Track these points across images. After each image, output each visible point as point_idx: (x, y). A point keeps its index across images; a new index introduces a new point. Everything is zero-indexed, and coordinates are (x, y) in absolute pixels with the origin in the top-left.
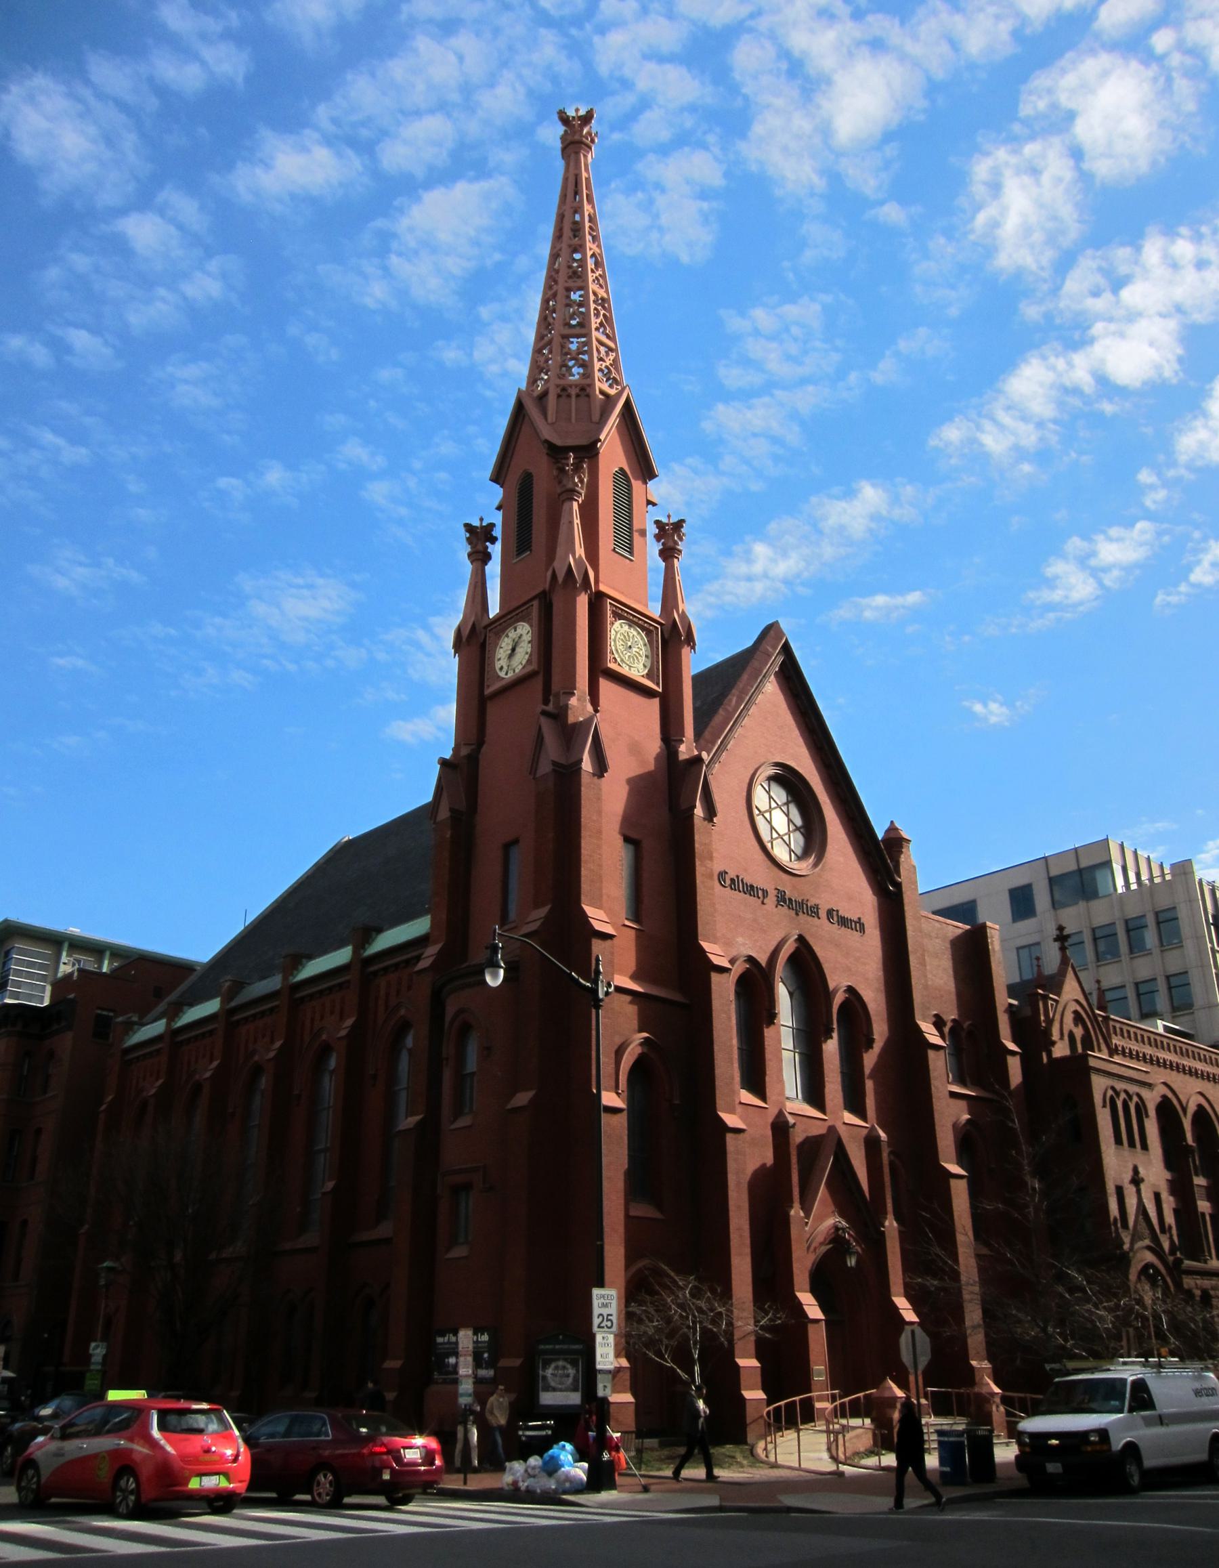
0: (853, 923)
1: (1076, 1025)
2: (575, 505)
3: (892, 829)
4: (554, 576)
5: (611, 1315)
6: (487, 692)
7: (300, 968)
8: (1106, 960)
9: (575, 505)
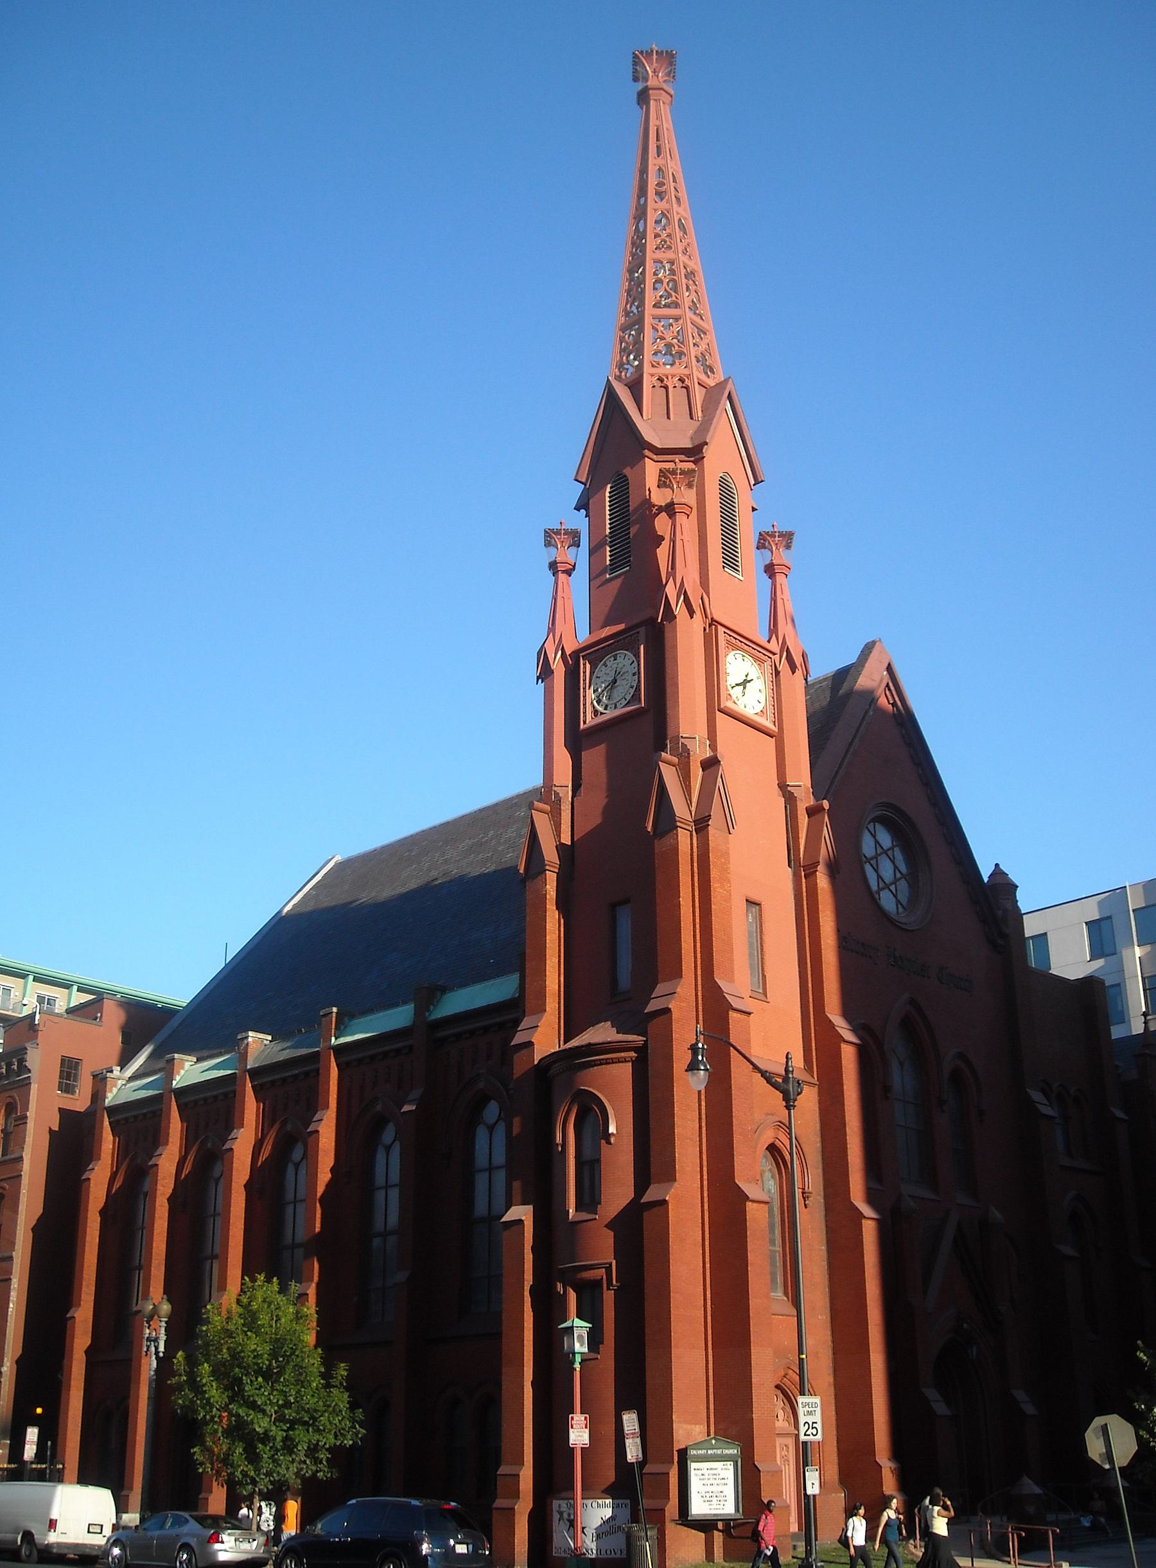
3: (998, 872)
5: (816, 1423)
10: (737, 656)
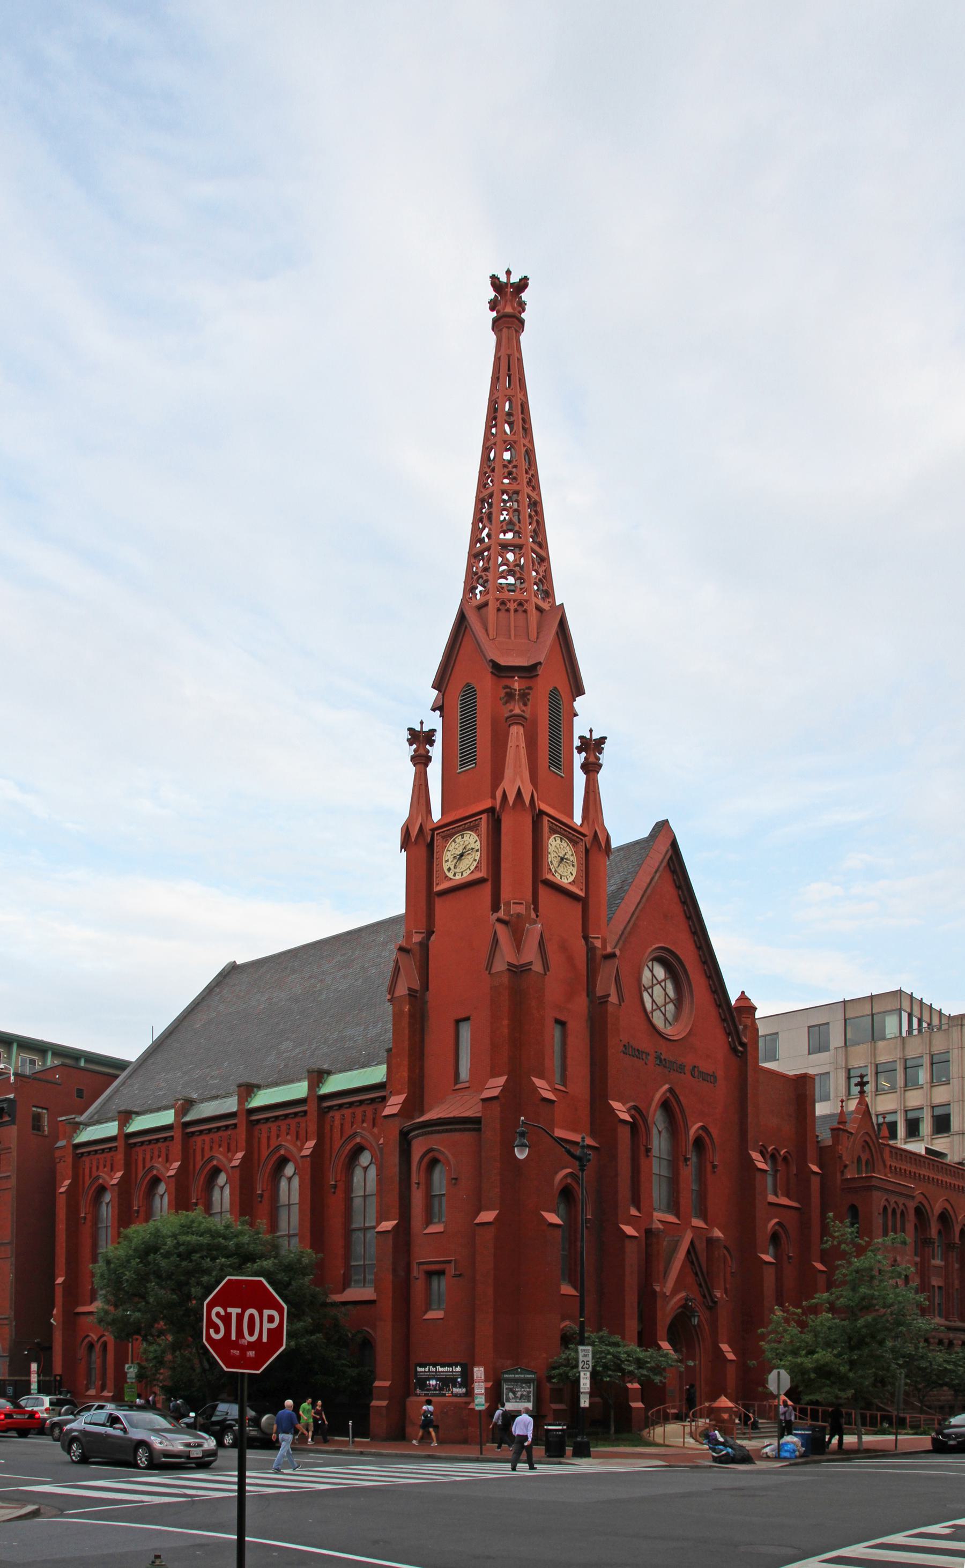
1: (864, 1151)
3: (743, 997)
4: (504, 796)
7: (253, 1095)
10: (557, 838)
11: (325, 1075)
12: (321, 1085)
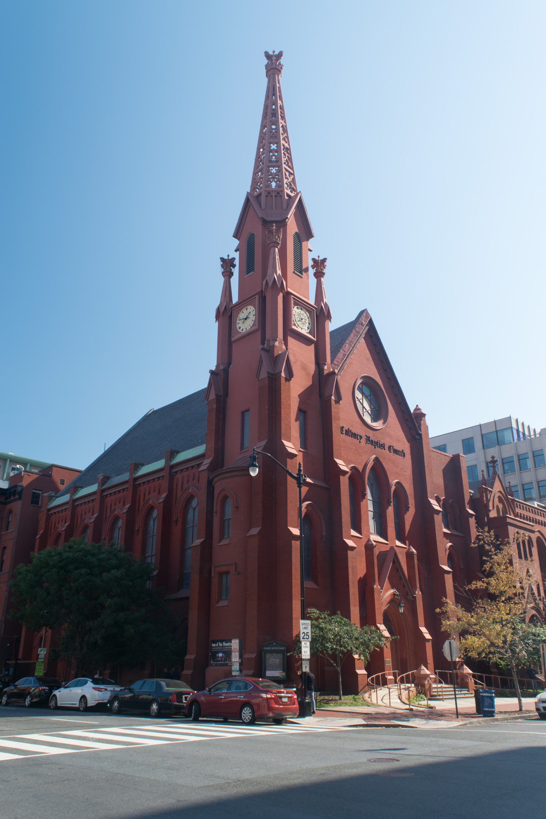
0: (400, 452)
2: (277, 250)
3: (417, 409)
4: (267, 283)
5: (308, 633)
6: (233, 339)
7: (138, 470)
8: (508, 473)
9: (277, 250)
11: (175, 454)
12: (172, 459)
